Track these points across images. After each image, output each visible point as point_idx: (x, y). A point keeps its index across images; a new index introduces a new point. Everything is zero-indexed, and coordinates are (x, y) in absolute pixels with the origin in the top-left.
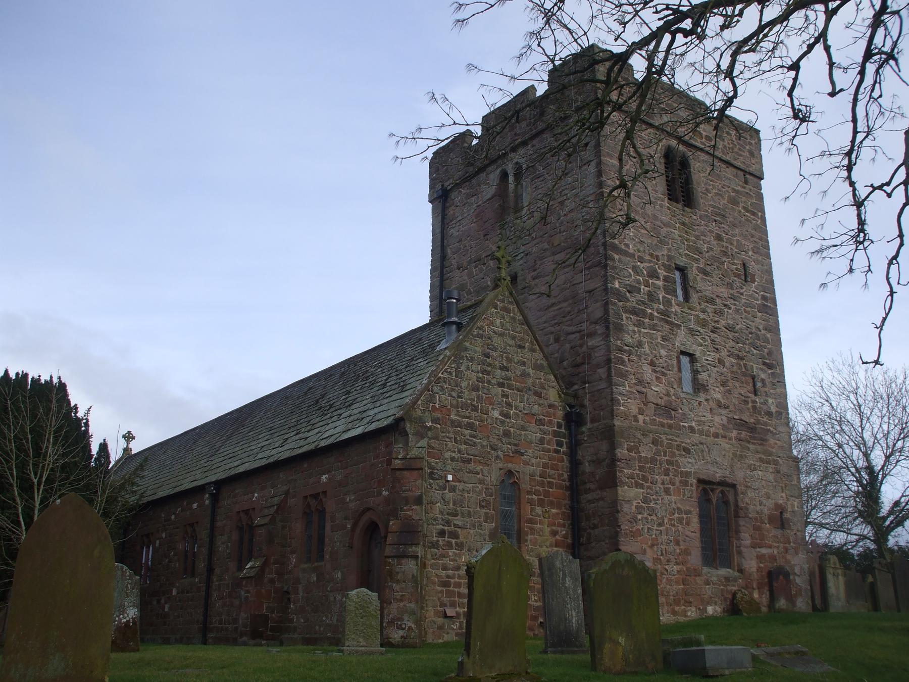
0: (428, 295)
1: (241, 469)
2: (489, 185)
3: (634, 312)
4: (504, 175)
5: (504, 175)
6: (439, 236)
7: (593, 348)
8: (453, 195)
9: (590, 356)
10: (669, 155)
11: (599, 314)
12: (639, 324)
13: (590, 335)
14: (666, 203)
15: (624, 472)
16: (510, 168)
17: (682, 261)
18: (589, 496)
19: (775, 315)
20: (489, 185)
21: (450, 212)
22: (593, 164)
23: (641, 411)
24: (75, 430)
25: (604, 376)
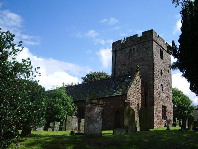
0: (111, 69)
1: (80, 100)
2: (127, 51)
3: (156, 77)
4: (131, 50)
5: (131, 50)
6: (114, 59)
7: (150, 83)
8: (118, 51)
9: (149, 84)
10: (161, 50)
11: (152, 77)
12: (157, 79)
13: (150, 81)
14: (160, 59)
15: (155, 104)
16: (132, 48)
17: (162, 69)
18: (148, 107)
19: (171, 79)
20: (127, 51)
21: (117, 54)
22: (152, 51)
23: (157, 94)
24: (44, 89)
25: (152, 88)
